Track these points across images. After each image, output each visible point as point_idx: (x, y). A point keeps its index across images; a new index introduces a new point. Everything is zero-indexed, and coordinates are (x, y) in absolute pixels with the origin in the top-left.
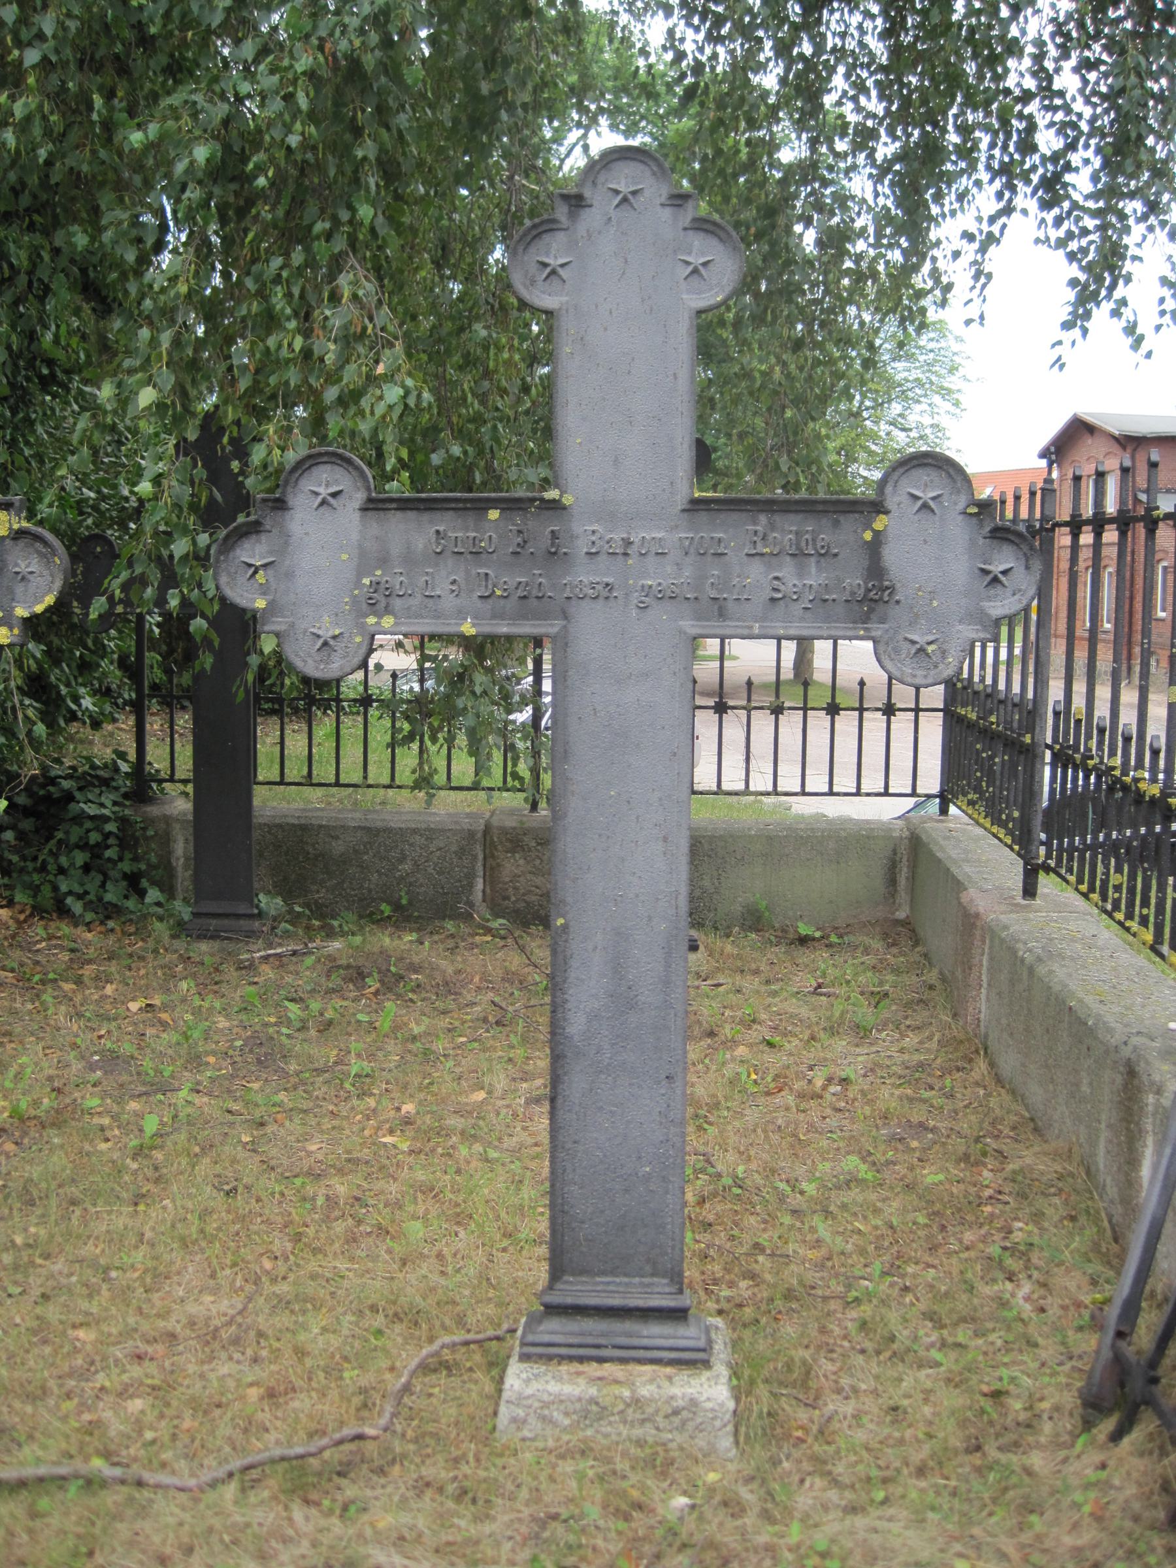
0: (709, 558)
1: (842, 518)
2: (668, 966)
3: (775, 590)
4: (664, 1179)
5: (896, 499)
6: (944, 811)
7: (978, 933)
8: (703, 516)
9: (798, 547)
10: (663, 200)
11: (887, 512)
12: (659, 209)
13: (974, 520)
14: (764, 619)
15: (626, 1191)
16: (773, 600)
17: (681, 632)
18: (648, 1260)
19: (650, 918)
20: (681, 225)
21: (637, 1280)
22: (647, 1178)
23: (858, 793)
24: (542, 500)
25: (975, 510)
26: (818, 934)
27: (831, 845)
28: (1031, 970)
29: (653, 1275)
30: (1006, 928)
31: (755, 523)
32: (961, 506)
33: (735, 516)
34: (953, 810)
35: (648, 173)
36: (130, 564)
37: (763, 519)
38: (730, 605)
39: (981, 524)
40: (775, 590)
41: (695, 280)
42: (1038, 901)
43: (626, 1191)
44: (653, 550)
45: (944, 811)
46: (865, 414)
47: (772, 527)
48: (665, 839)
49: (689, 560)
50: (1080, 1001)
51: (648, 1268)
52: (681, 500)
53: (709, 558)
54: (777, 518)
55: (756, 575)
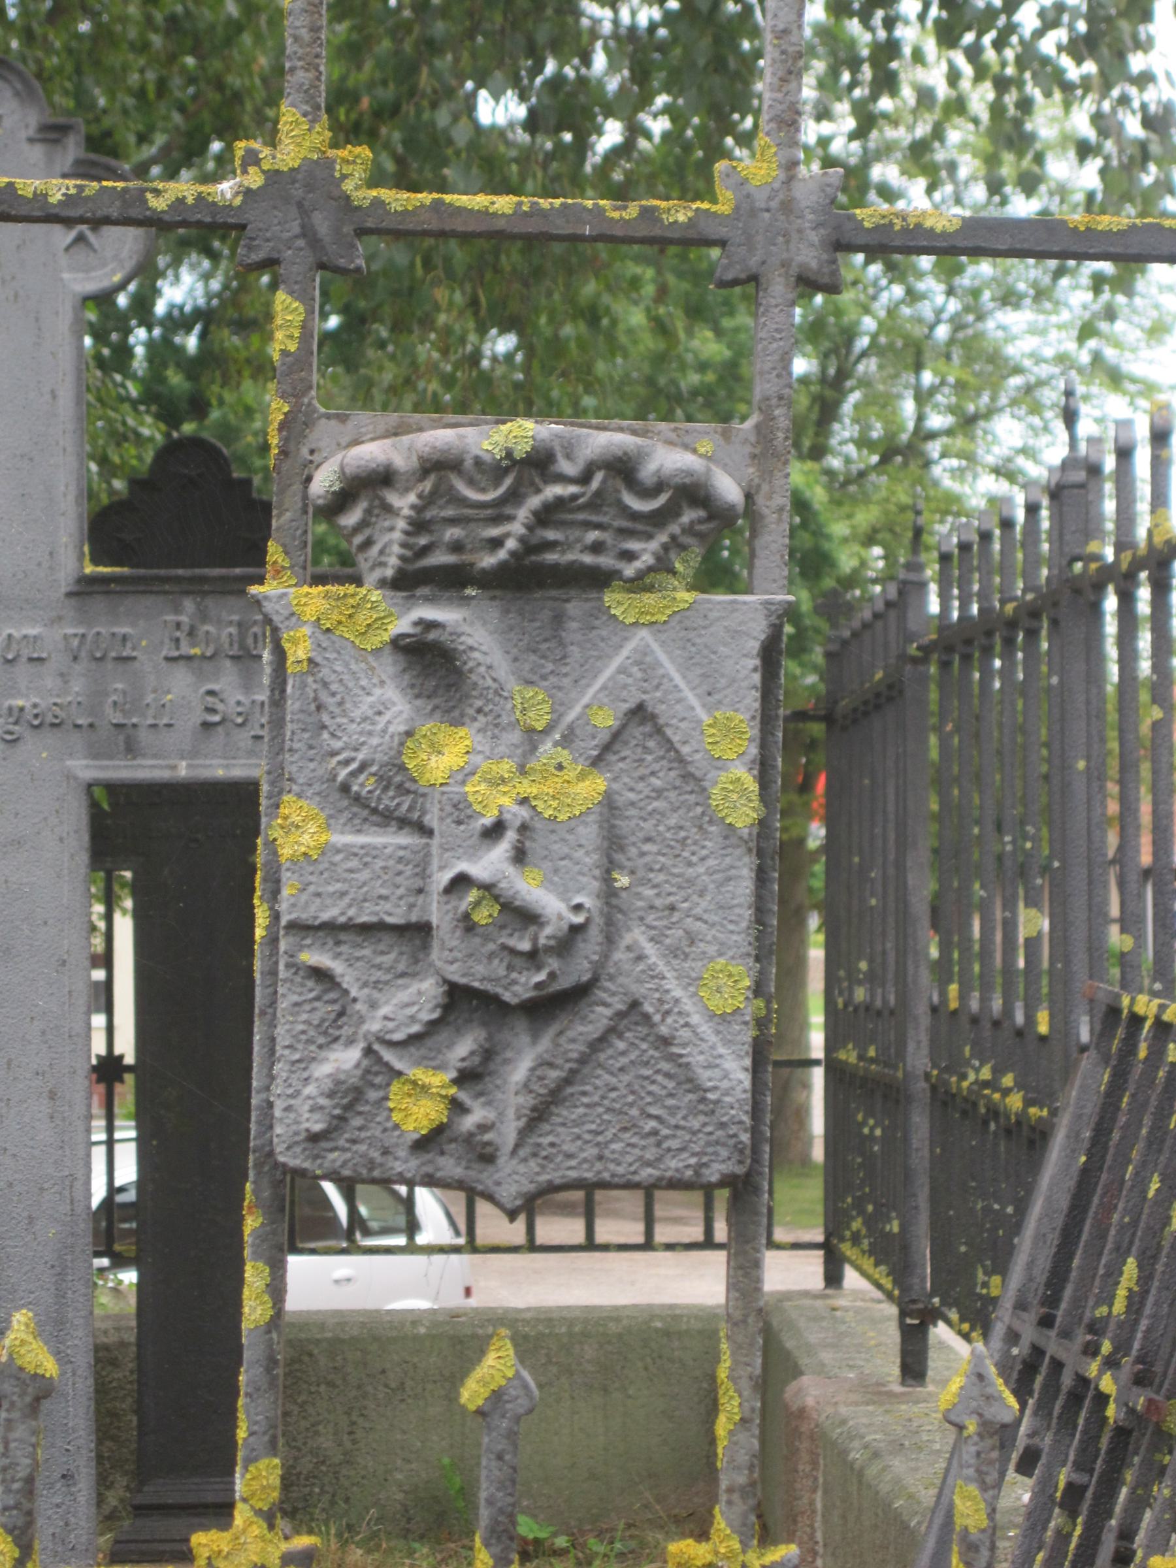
0: (110, 665)
2: (60, 1295)
3: (211, 710)
6: (833, 1278)
7: (804, 1445)
8: (99, 604)
9: (243, 646)
10: (31, 132)
12: (26, 147)
14: (194, 754)
16: (206, 725)
17: (69, 776)
20: (58, 169)
23: (648, 1245)
24: (1128, 1253)
26: (561, 1542)
27: (590, 1352)
28: (860, 1474)
30: (843, 1422)
31: (177, 610)
33: (148, 601)
34: (852, 1278)
35: (8, 93)
37: (189, 604)
38: (143, 736)
40: (211, 710)
41: (80, 253)
44: (25, 653)
45: (833, 1278)
46: (934, 449)
47: (204, 617)
48: (52, 1095)
49: (78, 668)
53: (110, 665)
54: (210, 602)
55: (181, 687)
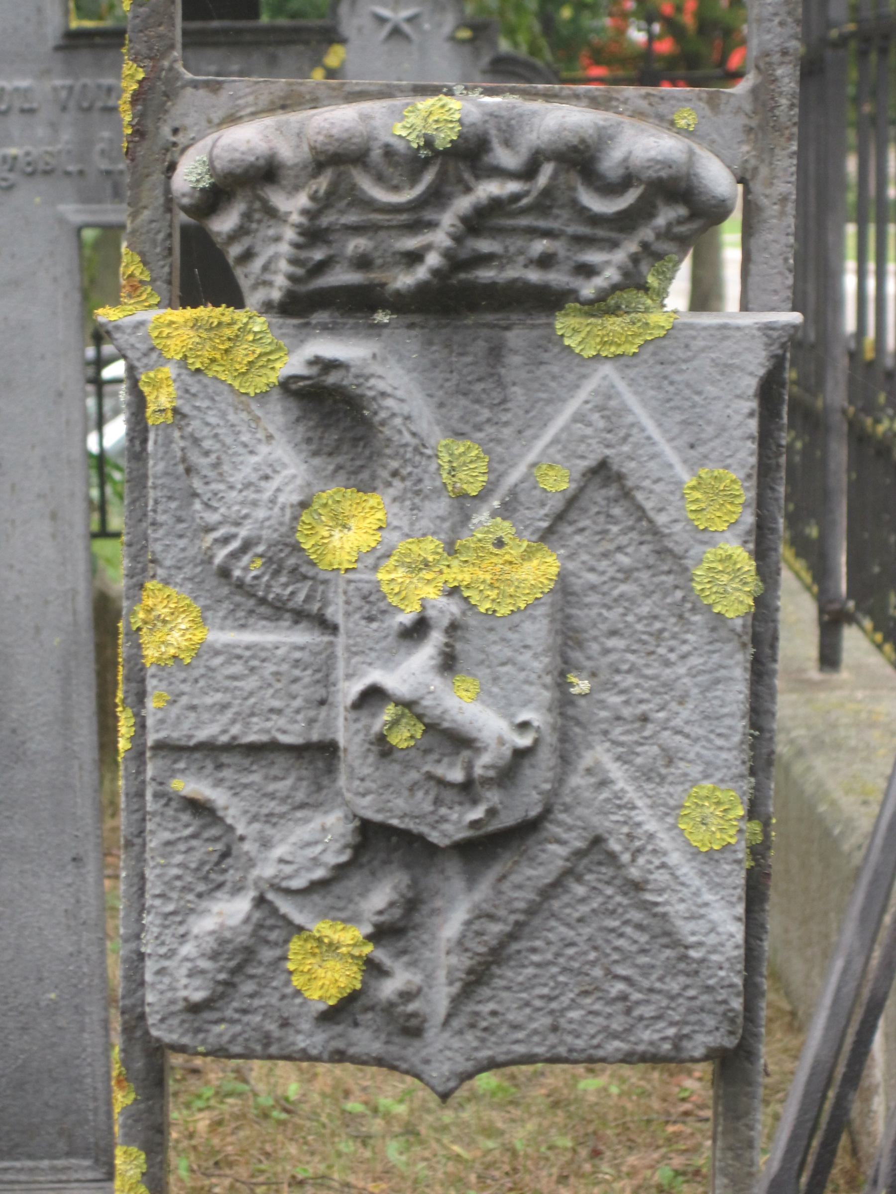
1: (280, 52)
4: (78, 1009)
5: (356, 22)
8: (85, 56)
11: (343, 41)
13: (467, 50)
15: (24, 1029)
17: (61, 221)
18: (61, 1133)
19: (38, 630)
21: (45, 1163)
22: (53, 1009)
25: (465, 34)
29: (69, 1154)
32: (447, 29)
36: (550, 1175)
39: (477, 53)
42: (844, 675)
43: (24, 1029)
44: (18, 104)
48: (54, 516)
49: (67, 117)
50: (833, 803)
51: (62, 1145)
52: (52, 32)
53: (96, 115)
